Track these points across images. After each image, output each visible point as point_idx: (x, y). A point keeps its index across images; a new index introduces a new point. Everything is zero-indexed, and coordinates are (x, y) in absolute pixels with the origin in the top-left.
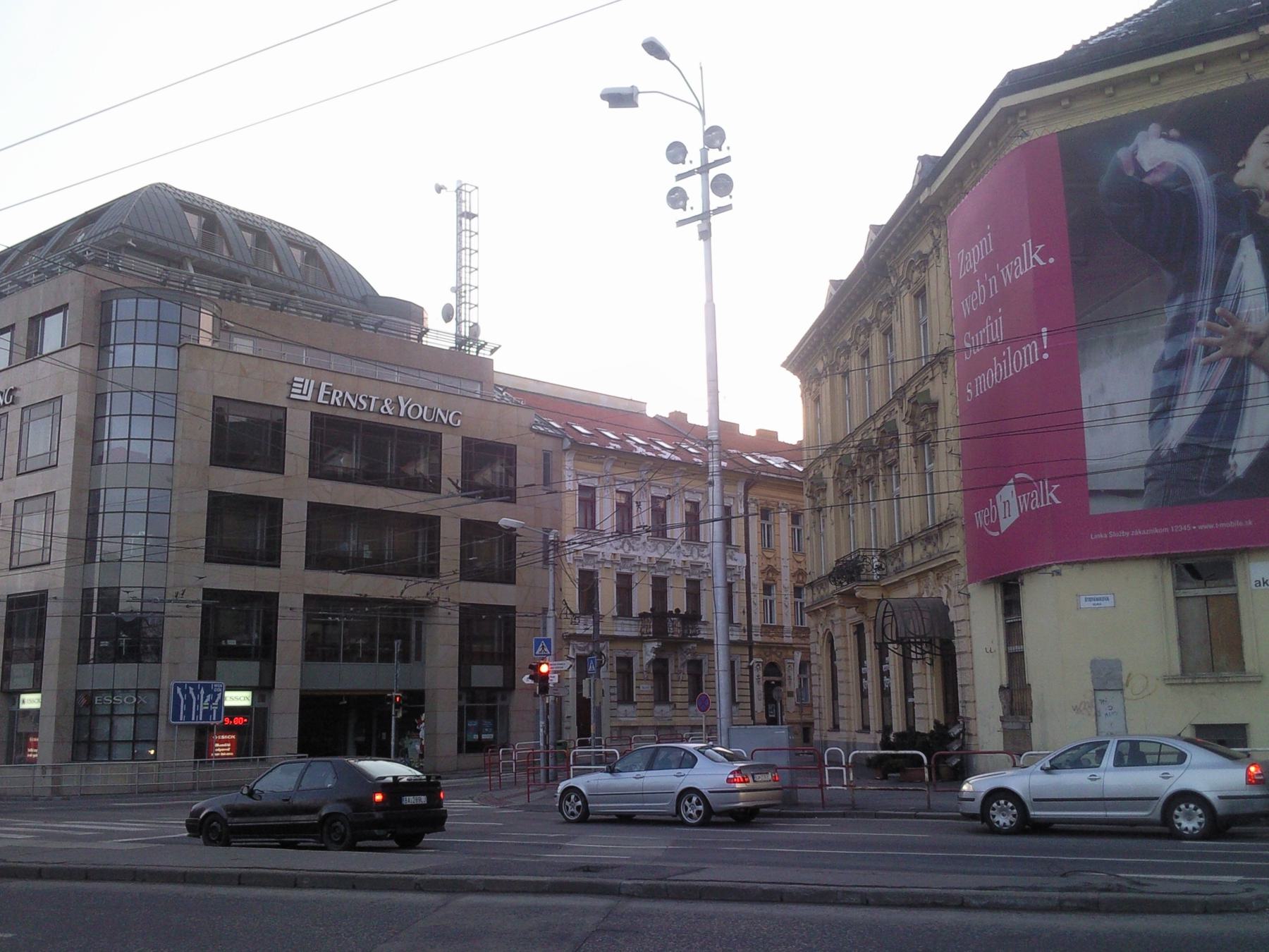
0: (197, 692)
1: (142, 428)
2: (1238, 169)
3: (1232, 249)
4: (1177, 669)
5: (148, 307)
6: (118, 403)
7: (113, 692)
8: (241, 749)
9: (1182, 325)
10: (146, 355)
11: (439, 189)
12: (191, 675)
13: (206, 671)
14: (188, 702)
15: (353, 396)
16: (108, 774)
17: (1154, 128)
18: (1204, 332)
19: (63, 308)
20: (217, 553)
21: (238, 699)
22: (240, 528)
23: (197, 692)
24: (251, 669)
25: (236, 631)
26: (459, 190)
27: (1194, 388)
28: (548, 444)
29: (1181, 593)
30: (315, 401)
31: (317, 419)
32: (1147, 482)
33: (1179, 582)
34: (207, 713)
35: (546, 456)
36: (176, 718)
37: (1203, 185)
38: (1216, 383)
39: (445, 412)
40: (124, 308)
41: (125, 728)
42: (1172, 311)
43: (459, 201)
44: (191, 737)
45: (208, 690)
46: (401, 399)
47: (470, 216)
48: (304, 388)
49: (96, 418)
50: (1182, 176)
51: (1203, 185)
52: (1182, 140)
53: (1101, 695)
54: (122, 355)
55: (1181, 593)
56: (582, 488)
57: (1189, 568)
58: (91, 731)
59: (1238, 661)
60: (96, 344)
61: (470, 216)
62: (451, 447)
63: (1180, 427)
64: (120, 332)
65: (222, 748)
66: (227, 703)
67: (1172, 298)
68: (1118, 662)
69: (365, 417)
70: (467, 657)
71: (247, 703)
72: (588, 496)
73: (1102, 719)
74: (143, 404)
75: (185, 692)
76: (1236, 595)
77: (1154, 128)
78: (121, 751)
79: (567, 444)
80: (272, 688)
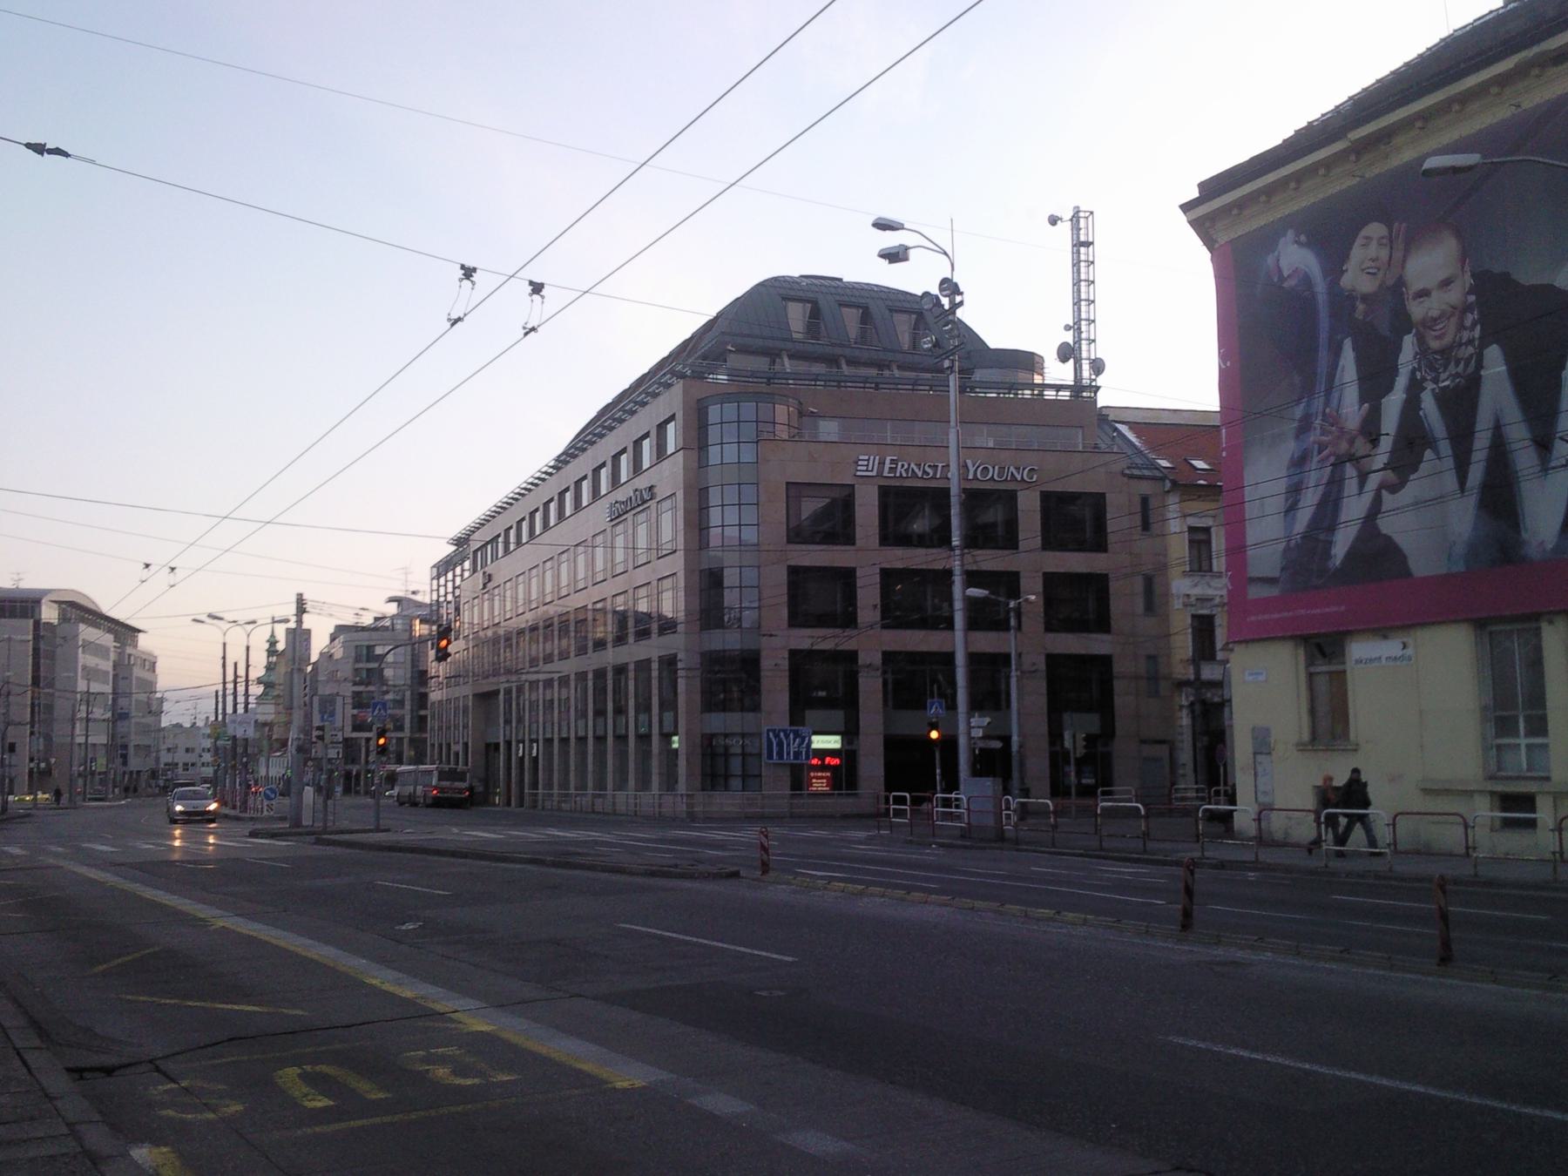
0: (787, 736)
1: (732, 516)
2: (1343, 272)
3: (1336, 351)
4: (1306, 737)
5: (730, 409)
6: (714, 497)
7: (726, 736)
8: (835, 783)
9: (1304, 427)
10: (731, 453)
11: (1054, 221)
12: (785, 724)
13: (796, 717)
14: (780, 744)
15: (919, 466)
16: (727, 801)
17: (1290, 234)
18: (1318, 431)
19: (672, 418)
20: (798, 617)
21: (831, 742)
22: (817, 596)
23: (787, 736)
24: (838, 716)
25: (822, 686)
26: (1075, 218)
27: (1312, 484)
28: (1145, 488)
29: (1312, 669)
30: (880, 474)
31: (884, 492)
32: (1283, 569)
33: (1310, 662)
34: (797, 755)
35: (1145, 501)
36: (770, 756)
37: (1320, 287)
38: (1325, 481)
39: (1018, 469)
40: (714, 413)
41: (736, 765)
42: (1299, 412)
43: (1076, 228)
44: (786, 774)
45: (797, 734)
46: (969, 462)
47: (1088, 244)
48: (868, 464)
49: (701, 509)
50: (1307, 281)
51: (1320, 287)
52: (1308, 245)
53: (1260, 758)
54: (714, 453)
55: (1312, 669)
56: (1192, 529)
57: (1319, 647)
58: (726, 768)
59: (1345, 734)
60: (695, 445)
61: (1088, 244)
62: (1029, 506)
63: (1304, 517)
64: (713, 434)
65: (820, 784)
66: (814, 746)
67: (1298, 401)
68: (1268, 730)
69: (934, 484)
70: (1057, 706)
71: (838, 746)
72: (1202, 537)
73: (1261, 780)
74: (731, 495)
75: (777, 736)
76: (1344, 672)
77: (1290, 234)
78: (736, 783)
79: (1168, 485)
80: (857, 733)
